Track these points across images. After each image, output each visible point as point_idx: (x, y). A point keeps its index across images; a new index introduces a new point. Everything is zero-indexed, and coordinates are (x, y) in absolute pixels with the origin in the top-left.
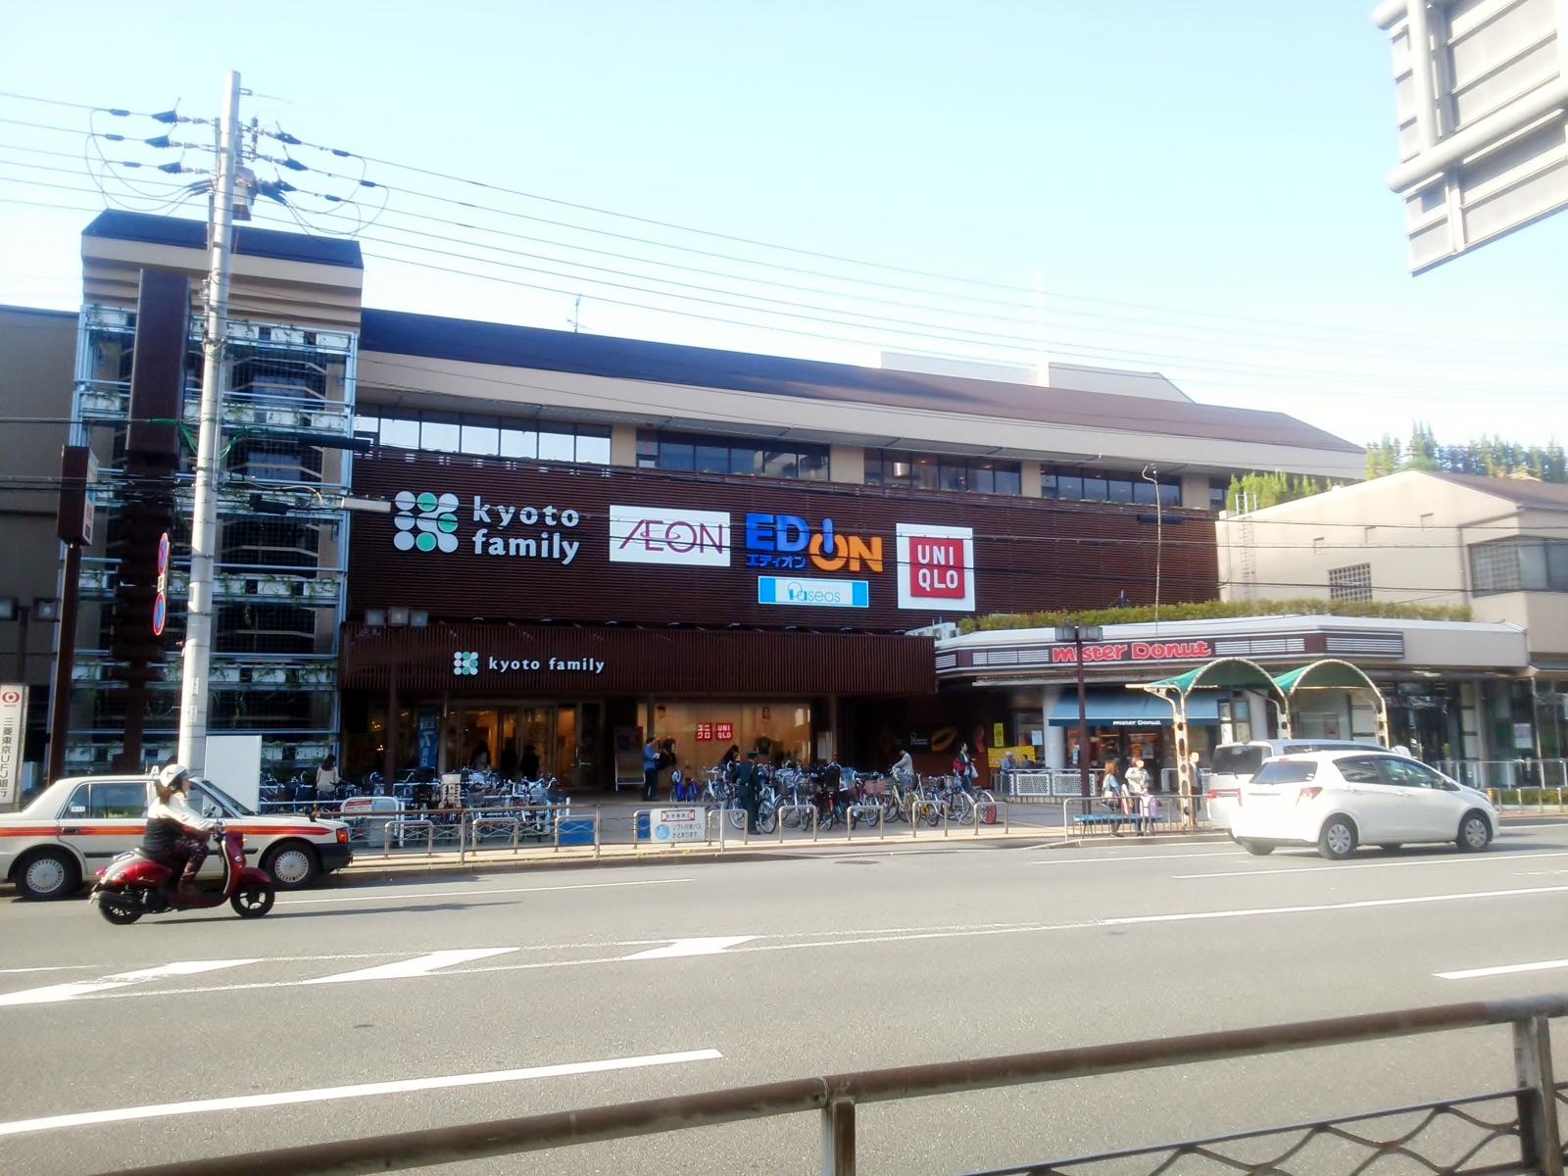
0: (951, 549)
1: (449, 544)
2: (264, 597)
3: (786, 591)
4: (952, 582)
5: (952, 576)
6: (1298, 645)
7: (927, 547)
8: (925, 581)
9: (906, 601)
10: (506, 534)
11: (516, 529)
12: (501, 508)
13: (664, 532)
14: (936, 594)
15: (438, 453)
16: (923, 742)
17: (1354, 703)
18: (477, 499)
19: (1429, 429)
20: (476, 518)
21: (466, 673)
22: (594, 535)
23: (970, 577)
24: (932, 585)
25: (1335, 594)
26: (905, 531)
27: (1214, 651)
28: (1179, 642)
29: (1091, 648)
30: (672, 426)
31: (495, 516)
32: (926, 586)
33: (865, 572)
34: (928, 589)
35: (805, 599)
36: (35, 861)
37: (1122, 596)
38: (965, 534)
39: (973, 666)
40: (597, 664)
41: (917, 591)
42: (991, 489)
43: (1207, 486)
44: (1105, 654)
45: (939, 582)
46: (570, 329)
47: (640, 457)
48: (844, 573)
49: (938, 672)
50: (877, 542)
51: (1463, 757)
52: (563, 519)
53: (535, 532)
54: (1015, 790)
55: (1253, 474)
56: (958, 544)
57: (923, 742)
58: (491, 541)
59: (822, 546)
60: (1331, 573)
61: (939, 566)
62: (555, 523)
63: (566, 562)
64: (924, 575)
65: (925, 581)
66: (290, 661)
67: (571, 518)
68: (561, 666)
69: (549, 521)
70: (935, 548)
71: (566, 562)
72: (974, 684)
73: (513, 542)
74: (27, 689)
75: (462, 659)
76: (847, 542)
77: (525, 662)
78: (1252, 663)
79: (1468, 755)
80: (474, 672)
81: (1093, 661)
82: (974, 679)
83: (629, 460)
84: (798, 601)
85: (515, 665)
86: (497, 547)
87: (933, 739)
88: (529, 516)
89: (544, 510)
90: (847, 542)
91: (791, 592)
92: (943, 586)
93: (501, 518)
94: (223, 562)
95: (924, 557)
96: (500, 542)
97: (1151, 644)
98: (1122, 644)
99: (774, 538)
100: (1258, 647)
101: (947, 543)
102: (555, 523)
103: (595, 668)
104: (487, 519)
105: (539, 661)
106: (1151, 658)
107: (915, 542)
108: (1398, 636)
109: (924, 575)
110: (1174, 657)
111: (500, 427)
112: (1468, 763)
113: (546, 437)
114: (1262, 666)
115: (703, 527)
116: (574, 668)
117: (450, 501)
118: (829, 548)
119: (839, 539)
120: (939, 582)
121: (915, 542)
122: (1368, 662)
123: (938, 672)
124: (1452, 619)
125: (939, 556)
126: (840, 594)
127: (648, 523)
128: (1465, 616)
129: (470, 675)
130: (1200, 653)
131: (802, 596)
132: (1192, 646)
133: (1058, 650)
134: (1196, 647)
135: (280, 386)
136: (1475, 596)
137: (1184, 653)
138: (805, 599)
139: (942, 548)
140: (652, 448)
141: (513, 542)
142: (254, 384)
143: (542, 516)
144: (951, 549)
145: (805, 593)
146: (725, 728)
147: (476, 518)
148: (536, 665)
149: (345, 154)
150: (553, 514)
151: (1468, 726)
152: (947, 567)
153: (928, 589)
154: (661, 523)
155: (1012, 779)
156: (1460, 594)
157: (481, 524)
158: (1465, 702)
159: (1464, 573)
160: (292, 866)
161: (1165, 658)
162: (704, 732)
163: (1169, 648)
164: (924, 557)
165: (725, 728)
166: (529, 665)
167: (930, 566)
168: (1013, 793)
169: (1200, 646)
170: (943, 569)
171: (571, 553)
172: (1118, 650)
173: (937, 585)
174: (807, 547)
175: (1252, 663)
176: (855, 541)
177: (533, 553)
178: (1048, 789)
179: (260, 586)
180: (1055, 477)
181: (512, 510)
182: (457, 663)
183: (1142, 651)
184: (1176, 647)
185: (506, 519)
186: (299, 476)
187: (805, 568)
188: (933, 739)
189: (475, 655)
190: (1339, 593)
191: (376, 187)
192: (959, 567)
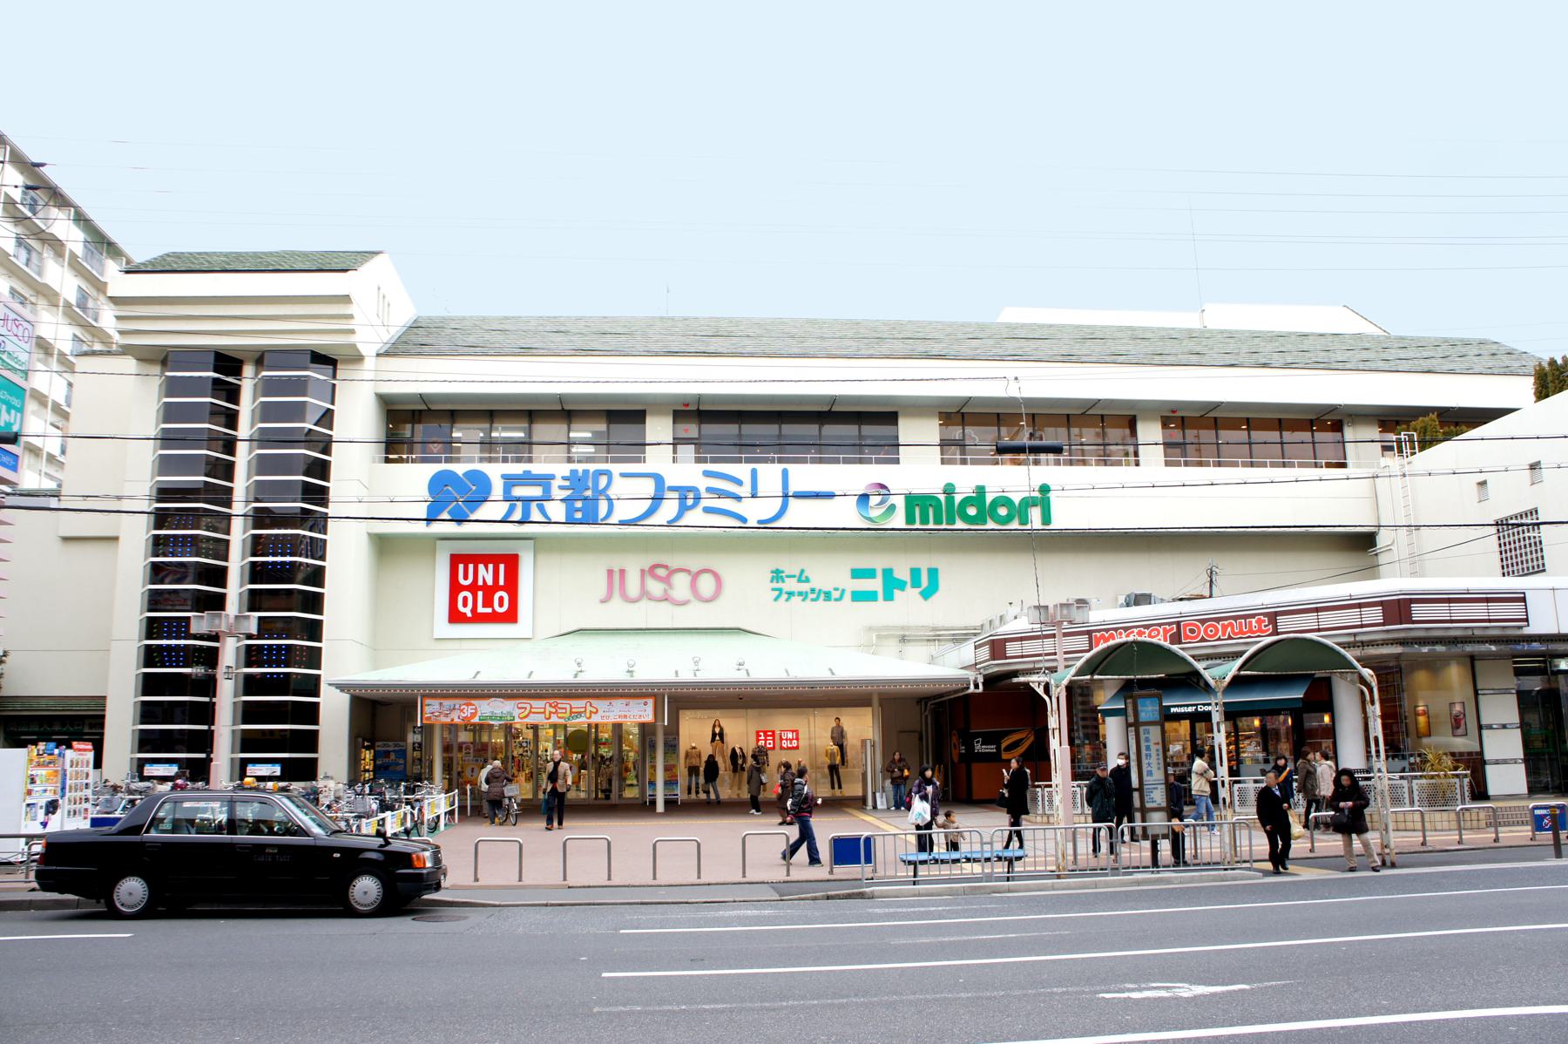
0: (502, 567)
4: (501, 605)
5: (501, 599)
6: (1375, 615)
7: (471, 567)
8: (465, 605)
16: (991, 749)
27: (1275, 628)
28: (1236, 618)
32: (468, 611)
34: (469, 615)
36: (133, 875)
39: (1007, 658)
45: (484, 606)
54: (1462, 787)
55: (1150, 432)
57: (991, 749)
61: (485, 587)
64: (465, 599)
65: (465, 605)
70: (481, 567)
72: (1015, 680)
78: (1181, 652)
87: (1003, 746)
92: (489, 610)
95: (466, 578)
97: (1203, 622)
100: (1328, 619)
106: (1203, 640)
109: (465, 599)
110: (1230, 638)
114: (1339, 644)
120: (484, 606)
122: (1402, 635)
132: (1251, 623)
133: (1098, 634)
134: (1254, 624)
137: (1241, 632)
139: (491, 566)
144: (502, 567)
153: (469, 615)
155: (1040, 794)
160: (130, 894)
161: (1219, 639)
162: (766, 740)
163: (1223, 625)
164: (466, 578)
165: (790, 736)
168: (1040, 812)
169: (1259, 622)
170: (489, 592)
172: (1165, 631)
173: (481, 609)
175: (1181, 652)
178: (1236, 793)
183: (1192, 631)
184: (1231, 624)
188: (1003, 746)
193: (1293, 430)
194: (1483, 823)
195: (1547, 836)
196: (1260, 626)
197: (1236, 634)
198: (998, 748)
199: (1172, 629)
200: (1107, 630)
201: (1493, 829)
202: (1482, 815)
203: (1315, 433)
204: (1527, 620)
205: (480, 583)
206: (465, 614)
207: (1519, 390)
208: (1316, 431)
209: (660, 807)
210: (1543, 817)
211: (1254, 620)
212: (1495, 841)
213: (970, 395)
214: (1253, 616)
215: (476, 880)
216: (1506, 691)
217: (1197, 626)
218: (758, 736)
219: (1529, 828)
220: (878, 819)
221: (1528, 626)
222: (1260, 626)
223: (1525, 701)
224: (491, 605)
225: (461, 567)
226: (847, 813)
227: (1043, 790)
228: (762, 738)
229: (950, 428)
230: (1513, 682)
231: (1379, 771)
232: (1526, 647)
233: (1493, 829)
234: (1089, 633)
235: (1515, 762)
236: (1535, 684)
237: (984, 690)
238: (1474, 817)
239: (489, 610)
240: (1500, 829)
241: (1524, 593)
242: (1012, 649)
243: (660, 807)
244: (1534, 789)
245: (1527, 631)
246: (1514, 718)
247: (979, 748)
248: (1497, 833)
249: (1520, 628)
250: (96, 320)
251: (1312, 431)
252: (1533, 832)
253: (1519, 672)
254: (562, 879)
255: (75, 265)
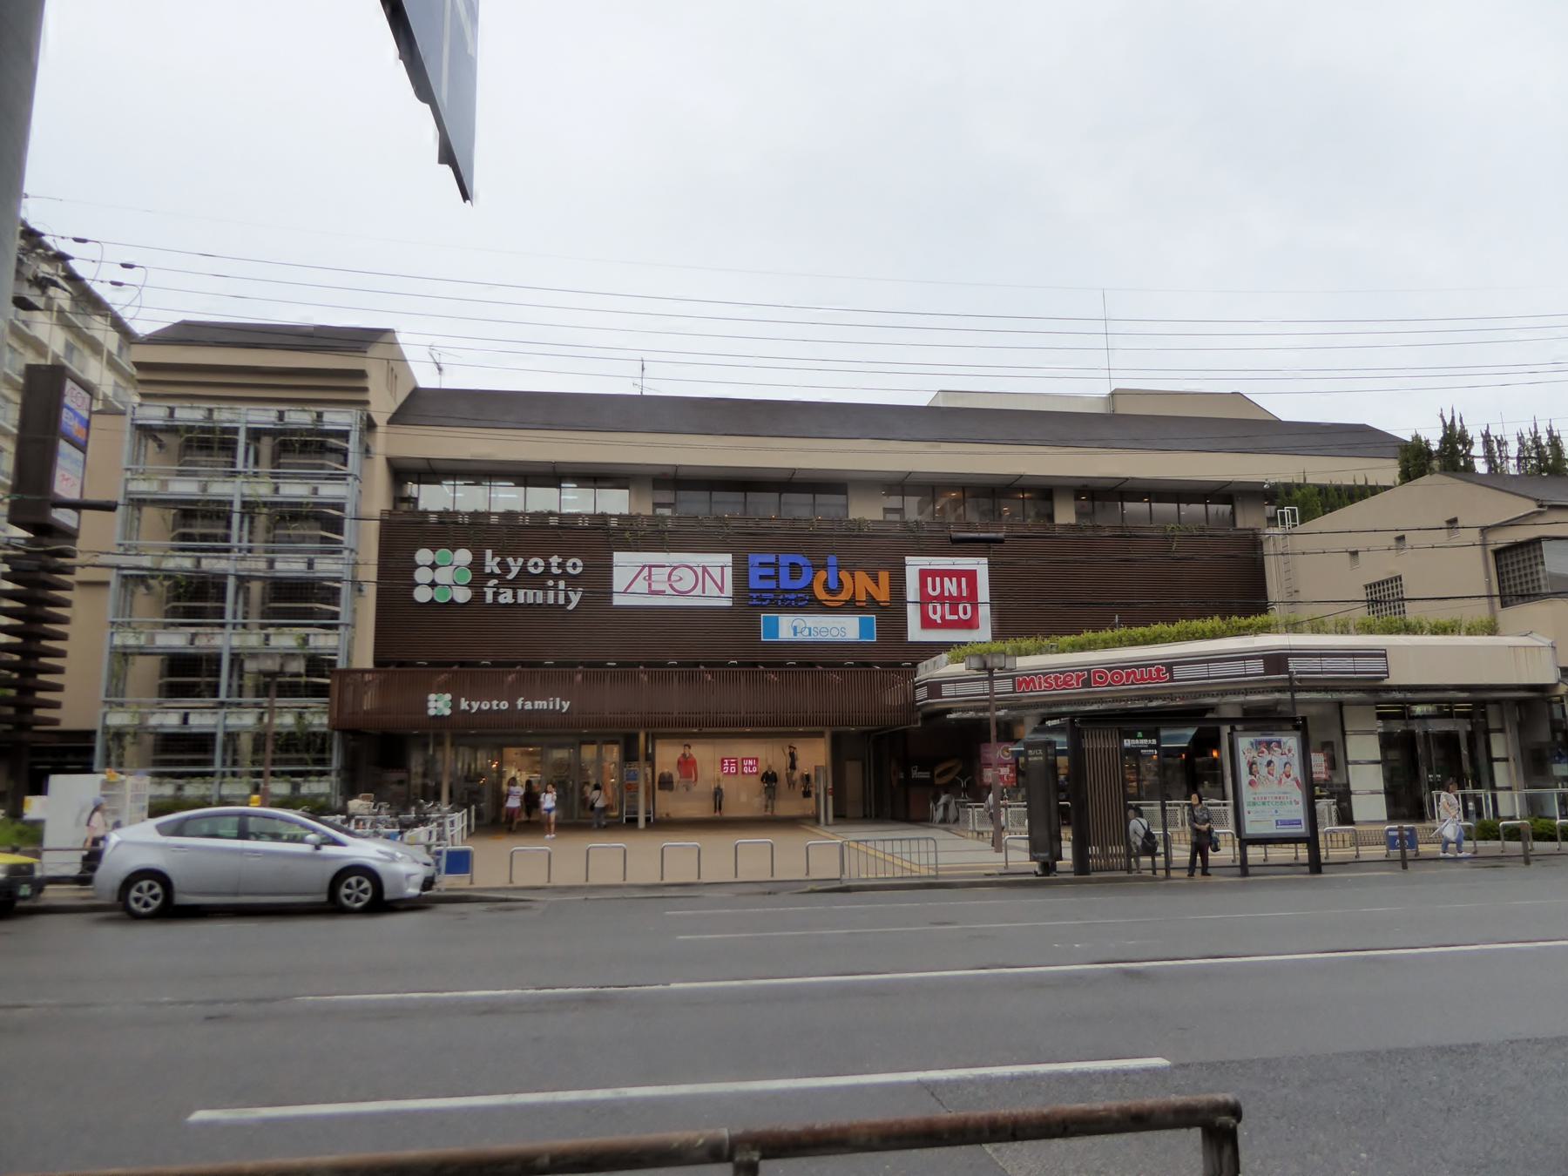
0: (964, 580)
1: (463, 595)
2: (316, 648)
3: (790, 627)
4: (965, 613)
6: (1257, 667)
7: (938, 579)
8: (935, 613)
9: (915, 633)
10: (514, 585)
11: (525, 579)
12: (510, 560)
13: (667, 576)
14: (947, 625)
15: (578, 515)
16: (925, 775)
17: (1347, 728)
18: (489, 553)
19: (1550, 432)
20: (488, 570)
21: (439, 714)
22: (598, 579)
23: (985, 612)
24: (943, 617)
25: (1371, 609)
26: (914, 566)
28: (1137, 667)
29: (1053, 676)
30: (681, 472)
31: (505, 568)
32: (937, 618)
33: (872, 605)
34: (939, 621)
35: (810, 635)
37: (1117, 620)
38: (980, 566)
40: (564, 703)
41: (927, 623)
42: (1149, 522)
43: (1073, 498)
44: (1066, 683)
46: (636, 392)
47: (656, 505)
48: (850, 607)
49: (918, 704)
50: (884, 577)
51: (1493, 787)
52: (581, 564)
53: (537, 582)
56: (971, 576)
57: (925, 775)
58: (501, 590)
59: (826, 583)
60: (1366, 588)
61: (951, 597)
62: (560, 571)
63: (570, 607)
65: (935, 613)
66: (211, 705)
67: (575, 566)
68: (528, 706)
69: (555, 571)
70: (946, 580)
71: (570, 607)
72: (948, 716)
73: (521, 593)
74: (324, 729)
75: (434, 566)
76: (853, 577)
77: (555, 560)
79: (1499, 783)
80: (447, 712)
81: (1054, 689)
82: (949, 711)
83: (647, 510)
84: (803, 637)
85: (485, 706)
86: (506, 597)
87: (936, 772)
88: (536, 565)
89: (551, 560)
90: (853, 577)
91: (795, 629)
92: (956, 617)
93: (510, 569)
94: (263, 618)
95: (934, 589)
96: (509, 593)
97: (1110, 669)
98: (1081, 671)
99: (776, 577)
101: (958, 574)
102: (560, 571)
103: (561, 707)
104: (497, 571)
105: (509, 703)
106: (1110, 685)
107: (924, 574)
108: (1382, 654)
110: (1133, 684)
111: (525, 485)
112: (1500, 794)
113: (534, 492)
115: (704, 568)
116: (541, 707)
117: (464, 556)
118: (833, 585)
119: (845, 576)
121: (924, 574)
123: (918, 704)
124: (1469, 632)
125: (951, 587)
126: (846, 628)
127: (650, 567)
128: (1492, 630)
129: (443, 716)
130: (1159, 677)
131: (806, 632)
132: (1150, 671)
134: (1153, 672)
135: (215, 459)
136: (1504, 605)
137: (1151, 678)
138: (810, 635)
139: (954, 579)
140: (666, 496)
141: (536, 703)
142: (282, 461)
143: (548, 566)
144: (964, 580)
145: (810, 629)
146: (750, 762)
147: (488, 570)
148: (504, 705)
149: (84, 241)
150: (559, 563)
151: (1497, 751)
152: (960, 598)
153: (939, 621)
154: (664, 566)
156: (1485, 601)
157: (492, 575)
158: (1493, 724)
159: (1490, 582)
161: (1124, 684)
162: (729, 767)
164: (934, 589)
165: (750, 762)
166: (498, 705)
167: (941, 599)
168: (971, 828)
169: (1158, 671)
170: (954, 602)
171: (575, 598)
172: (1078, 677)
173: (949, 617)
174: (811, 585)
176: (861, 576)
177: (545, 707)
179: (311, 639)
180: (901, 497)
181: (521, 561)
182: (431, 704)
183: (1101, 677)
185: (515, 571)
186: (318, 540)
187: (807, 603)
188: (936, 772)
189: (448, 697)
190: (1375, 609)
191: (136, 268)
192: (972, 597)
193: (1188, 502)
194: (1347, 843)
195: (1396, 853)
196: (1158, 674)
197: (1137, 680)
198: (932, 774)
199: (1084, 675)
200: (1028, 675)
201: (1354, 848)
202: (1347, 837)
203: (1209, 506)
204: (1387, 673)
205: (947, 594)
206: (936, 620)
207: (1386, 471)
208: (1209, 503)
209: (642, 823)
210: (1395, 838)
211: (1153, 669)
212: (1264, 860)
213: (910, 469)
214: (1153, 665)
215: (511, 882)
216: (1371, 732)
217: (1106, 674)
218: (723, 762)
219: (1384, 847)
220: (833, 834)
221: (1388, 677)
222: (1158, 674)
223: (1387, 742)
224: (957, 613)
225: (929, 579)
226: (808, 831)
227: (1006, 809)
228: (727, 764)
229: (891, 497)
230: (1379, 726)
231: (1255, 799)
232: (1385, 696)
233: (1354, 848)
234: (1013, 677)
235: (1380, 793)
236: (1398, 727)
237: (922, 724)
238: (1340, 838)
239: (956, 617)
240: (1360, 848)
241: (1385, 650)
242: (947, 690)
243: (642, 823)
244: (1392, 817)
245: (1387, 682)
246: (1376, 754)
247: (916, 774)
248: (1357, 850)
249: (1382, 679)
250: (82, 372)
251: (1206, 504)
252: (1387, 850)
253: (1381, 716)
254: (546, 880)
255: (64, 321)
